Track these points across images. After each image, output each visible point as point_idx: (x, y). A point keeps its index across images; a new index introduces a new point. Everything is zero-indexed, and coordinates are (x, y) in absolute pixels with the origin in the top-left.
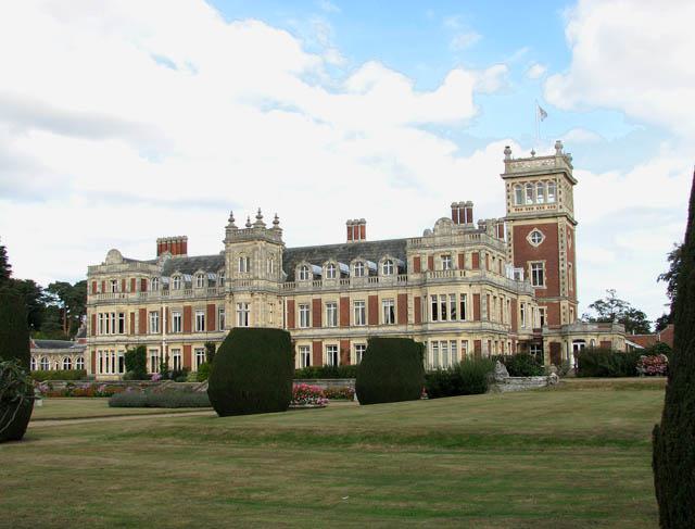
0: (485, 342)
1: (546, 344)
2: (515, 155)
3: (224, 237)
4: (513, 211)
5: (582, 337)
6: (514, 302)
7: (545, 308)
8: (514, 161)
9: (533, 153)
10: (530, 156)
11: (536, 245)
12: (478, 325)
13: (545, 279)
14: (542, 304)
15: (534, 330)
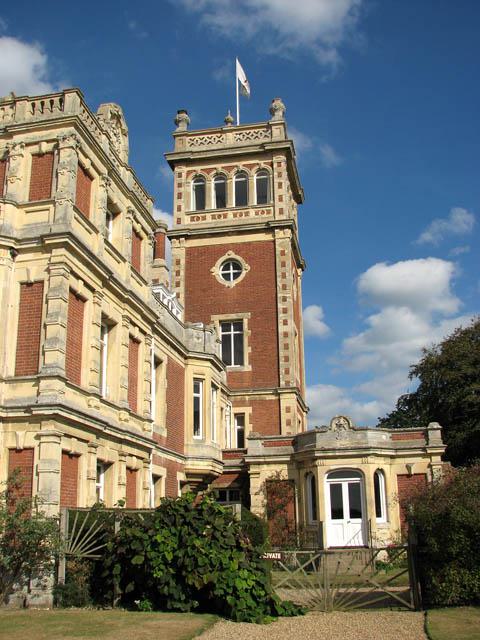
0: (49, 454)
1: (256, 483)
5: (354, 463)
6: (175, 377)
7: (247, 411)
11: (233, 283)
12: (25, 392)
13: (247, 350)
14: (242, 403)
15: (227, 453)
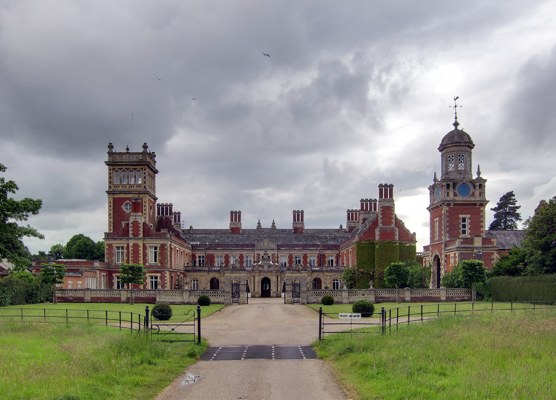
3: (428, 205)
4: (113, 187)
8: (116, 153)
9: (128, 149)
10: (126, 151)
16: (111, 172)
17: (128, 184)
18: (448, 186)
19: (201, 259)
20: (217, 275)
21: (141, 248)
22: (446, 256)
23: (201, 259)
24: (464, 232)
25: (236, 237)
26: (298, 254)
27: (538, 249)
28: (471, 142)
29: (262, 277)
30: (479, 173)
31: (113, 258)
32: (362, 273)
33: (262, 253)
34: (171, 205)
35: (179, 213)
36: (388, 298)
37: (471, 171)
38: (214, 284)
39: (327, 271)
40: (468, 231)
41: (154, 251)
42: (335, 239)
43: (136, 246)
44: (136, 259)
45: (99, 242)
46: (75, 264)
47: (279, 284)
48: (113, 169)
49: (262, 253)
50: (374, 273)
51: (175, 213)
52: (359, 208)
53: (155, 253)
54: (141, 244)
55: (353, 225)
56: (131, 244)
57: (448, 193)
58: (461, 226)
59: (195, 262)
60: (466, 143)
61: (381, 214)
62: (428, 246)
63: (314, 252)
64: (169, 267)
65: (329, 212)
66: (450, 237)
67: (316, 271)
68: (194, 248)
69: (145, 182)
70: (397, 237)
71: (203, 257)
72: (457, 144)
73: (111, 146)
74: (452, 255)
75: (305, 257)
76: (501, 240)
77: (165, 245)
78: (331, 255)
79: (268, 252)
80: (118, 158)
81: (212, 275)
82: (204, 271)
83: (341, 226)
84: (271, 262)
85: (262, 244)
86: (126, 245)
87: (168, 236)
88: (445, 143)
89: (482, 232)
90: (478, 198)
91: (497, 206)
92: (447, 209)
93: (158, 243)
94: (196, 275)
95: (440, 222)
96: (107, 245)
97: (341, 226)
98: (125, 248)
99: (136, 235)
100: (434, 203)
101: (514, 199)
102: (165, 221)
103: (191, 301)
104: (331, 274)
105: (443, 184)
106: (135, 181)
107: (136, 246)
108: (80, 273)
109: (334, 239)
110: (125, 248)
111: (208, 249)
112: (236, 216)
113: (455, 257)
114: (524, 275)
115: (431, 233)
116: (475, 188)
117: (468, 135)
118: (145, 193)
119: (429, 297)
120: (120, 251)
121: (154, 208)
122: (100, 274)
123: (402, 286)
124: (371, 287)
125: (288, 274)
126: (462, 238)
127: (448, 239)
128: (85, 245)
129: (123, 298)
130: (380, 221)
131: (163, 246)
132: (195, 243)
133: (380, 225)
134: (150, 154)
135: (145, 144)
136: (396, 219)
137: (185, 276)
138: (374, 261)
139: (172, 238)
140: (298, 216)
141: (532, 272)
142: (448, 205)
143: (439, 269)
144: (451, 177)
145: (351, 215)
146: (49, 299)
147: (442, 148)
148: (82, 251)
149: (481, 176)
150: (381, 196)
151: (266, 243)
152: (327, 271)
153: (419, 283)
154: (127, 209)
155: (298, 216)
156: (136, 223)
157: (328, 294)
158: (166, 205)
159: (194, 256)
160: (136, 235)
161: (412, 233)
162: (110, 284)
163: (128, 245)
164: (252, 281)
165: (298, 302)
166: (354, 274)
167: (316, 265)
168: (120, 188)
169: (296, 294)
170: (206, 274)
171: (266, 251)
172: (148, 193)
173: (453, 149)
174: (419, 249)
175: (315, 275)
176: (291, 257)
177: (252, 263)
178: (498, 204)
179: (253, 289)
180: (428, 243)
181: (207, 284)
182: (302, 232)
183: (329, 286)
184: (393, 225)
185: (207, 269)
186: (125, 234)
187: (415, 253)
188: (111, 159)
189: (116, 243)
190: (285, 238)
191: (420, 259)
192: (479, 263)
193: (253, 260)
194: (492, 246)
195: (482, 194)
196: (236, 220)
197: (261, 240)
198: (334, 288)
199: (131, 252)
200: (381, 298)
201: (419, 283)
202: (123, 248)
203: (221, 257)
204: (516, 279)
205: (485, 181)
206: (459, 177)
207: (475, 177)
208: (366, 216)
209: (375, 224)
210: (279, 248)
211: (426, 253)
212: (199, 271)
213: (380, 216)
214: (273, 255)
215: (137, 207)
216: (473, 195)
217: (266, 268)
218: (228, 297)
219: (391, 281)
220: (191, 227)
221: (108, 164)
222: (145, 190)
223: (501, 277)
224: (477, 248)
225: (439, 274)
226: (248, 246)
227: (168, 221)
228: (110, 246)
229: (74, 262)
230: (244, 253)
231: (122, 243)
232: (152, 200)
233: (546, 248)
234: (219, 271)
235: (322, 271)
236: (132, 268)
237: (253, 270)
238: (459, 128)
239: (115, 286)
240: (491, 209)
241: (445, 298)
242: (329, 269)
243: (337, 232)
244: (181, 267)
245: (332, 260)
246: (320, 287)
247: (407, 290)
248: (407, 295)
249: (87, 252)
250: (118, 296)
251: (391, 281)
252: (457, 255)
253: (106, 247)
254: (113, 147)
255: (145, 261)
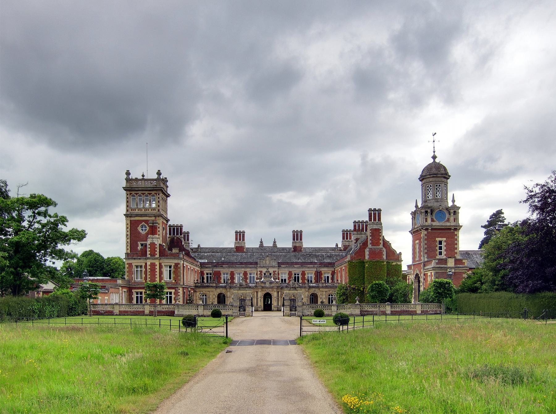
2: (133, 176)
4: (130, 211)
8: (132, 180)
10: (141, 177)
16: (129, 196)
17: (144, 208)
18: (426, 212)
19: (209, 276)
20: (223, 291)
21: (158, 267)
22: (424, 275)
23: (209, 276)
24: (440, 253)
25: (240, 255)
26: (297, 270)
27: (491, 271)
28: (447, 174)
29: (264, 293)
30: (453, 201)
31: (133, 276)
32: (354, 289)
33: (264, 270)
34: (181, 227)
35: (188, 233)
36: (372, 311)
37: (447, 199)
38: (221, 299)
39: (323, 287)
40: (444, 253)
41: (169, 269)
42: (331, 257)
43: (153, 265)
44: (153, 278)
45: (108, 258)
46: (107, 282)
47: (280, 299)
48: (130, 194)
49: (264, 270)
50: (364, 289)
51: (185, 233)
52: (352, 229)
53: (170, 271)
54: (157, 263)
55: (347, 244)
56: (149, 263)
57: (426, 219)
58: (438, 248)
59: (203, 278)
60: (442, 174)
61: (371, 236)
62: (411, 265)
63: (311, 269)
64: (182, 283)
65: (324, 236)
66: (427, 258)
67: (313, 287)
68: (202, 265)
69: (159, 206)
70: (385, 257)
71: (211, 274)
72: (435, 175)
73: (128, 173)
74: (429, 274)
75: (303, 274)
76: (477, 260)
77: (179, 264)
78: (326, 272)
79: (269, 270)
80: (134, 184)
81: (219, 291)
82: (212, 287)
83: (337, 245)
84: (272, 279)
85: (264, 262)
86: (144, 264)
87: (181, 256)
88: (424, 174)
89: (456, 253)
90: (453, 224)
91: (487, 223)
92: (426, 233)
93: (173, 262)
94: (205, 291)
95: (420, 245)
96: (127, 264)
97: (337, 245)
98: (143, 267)
99: (153, 255)
100: (416, 227)
101: (503, 217)
102: (177, 240)
103: (205, 314)
104: (327, 290)
105: (422, 211)
106: (150, 205)
107: (153, 265)
108: (107, 289)
109: (330, 257)
110: (143, 267)
111: (216, 266)
112: (240, 236)
113: (431, 276)
114: (480, 293)
115: (413, 254)
116: (450, 214)
117: (444, 167)
118: (159, 216)
119: (407, 311)
120: (139, 269)
121: (166, 229)
122: (122, 290)
123: (383, 301)
124: (357, 302)
125: (286, 291)
126: (437, 259)
127: (426, 260)
128: (95, 260)
129: (147, 312)
130: (369, 242)
131: (177, 265)
132: (203, 261)
133: (370, 246)
134: (163, 180)
135: (159, 171)
136: (384, 240)
137: (195, 291)
138: (364, 278)
139: (185, 257)
140: (297, 236)
141: (486, 290)
142: (427, 229)
143: (419, 286)
144: (429, 205)
145: (346, 234)
146: (84, 313)
147: (422, 178)
148: (92, 267)
149: (455, 204)
150: (370, 219)
151: (267, 261)
152: (323, 287)
153: (403, 299)
154: (142, 230)
155: (297, 236)
156: (153, 245)
157: (319, 308)
158: (177, 226)
159: (202, 273)
160: (153, 255)
161: (398, 253)
162: (130, 299)
163: (146, 264)
164: (256, 296)
165: (295, 315)
166: (347, 290)
167: (313, 281)
168: (137, 211)
169: (293, 308)
170: (214, 290)
171: (268, 269)
172: (161, 216)
173: (431, 179)
174: (404, 268)
175: (312, 291)
176: (290, 274)
177: (255, 280)
178: (488, 221)
179: (256, 303)
180: (410, 262)
181: (214, 299)
182: (301, 251)
183: (324, 300)
184: (381, 246)
185: (214, 285)
186: (143, 254)
187: (401, 271)
188: (128, 184)
189: (135, 262)
190: (285, 256)
191: (405, 277)
192: (447, 282)
193: (256, 276)
194: (463, 266)
195: (456, 219)
196: (240, 240)
197: (263, 258)
198: (329, 303)
199: (148, 270)
200: (365, 311)
201: (403, 299)
202: (141, 267)
203: (227, 274)
204: (474, 295)
205: (459, 208)
206: (436, 205)
207: (450, 204)
208: (359, 236)
209: (365, 244)
210: (279, 265)
211: (410, 271)
212: (208, 287)
213: (370, 238)
214: (274, 272)
215: (153, 230)
216: (448, 220)
217: (268, 285)
218: (236, 310)
219: (373, 297)
220: (199, 246)
221: (126, 189)
222: (158, 213)
223: (465, 294)
224: (449, 268)
225: (419, 290)
226: (251, 263)
227: (179, 241)
228: (130, 265)
229: (100, 279)
230: (248, 270)
231: (141, 262)
232: (165, 222)
233: (496, 271)
234: (225, 287)
235: (318, 287)
236: (155, 286)
237: (256, 286)
238: (437, 160)
239: (135, 301)
240: (482, 226)
241: (420, 312)
242: (324, 285)
243: (333, 250)
244: (192, 283)
245: (328, 277)
246: (317, 302)
247: (388, 305)
248: (388, 309)
249: (97, 267)
250: (142, 310)
251: (373, 297)
252: (433, 274)
253: (127, 266)
254: (129, 174)
255: (161, 278)
